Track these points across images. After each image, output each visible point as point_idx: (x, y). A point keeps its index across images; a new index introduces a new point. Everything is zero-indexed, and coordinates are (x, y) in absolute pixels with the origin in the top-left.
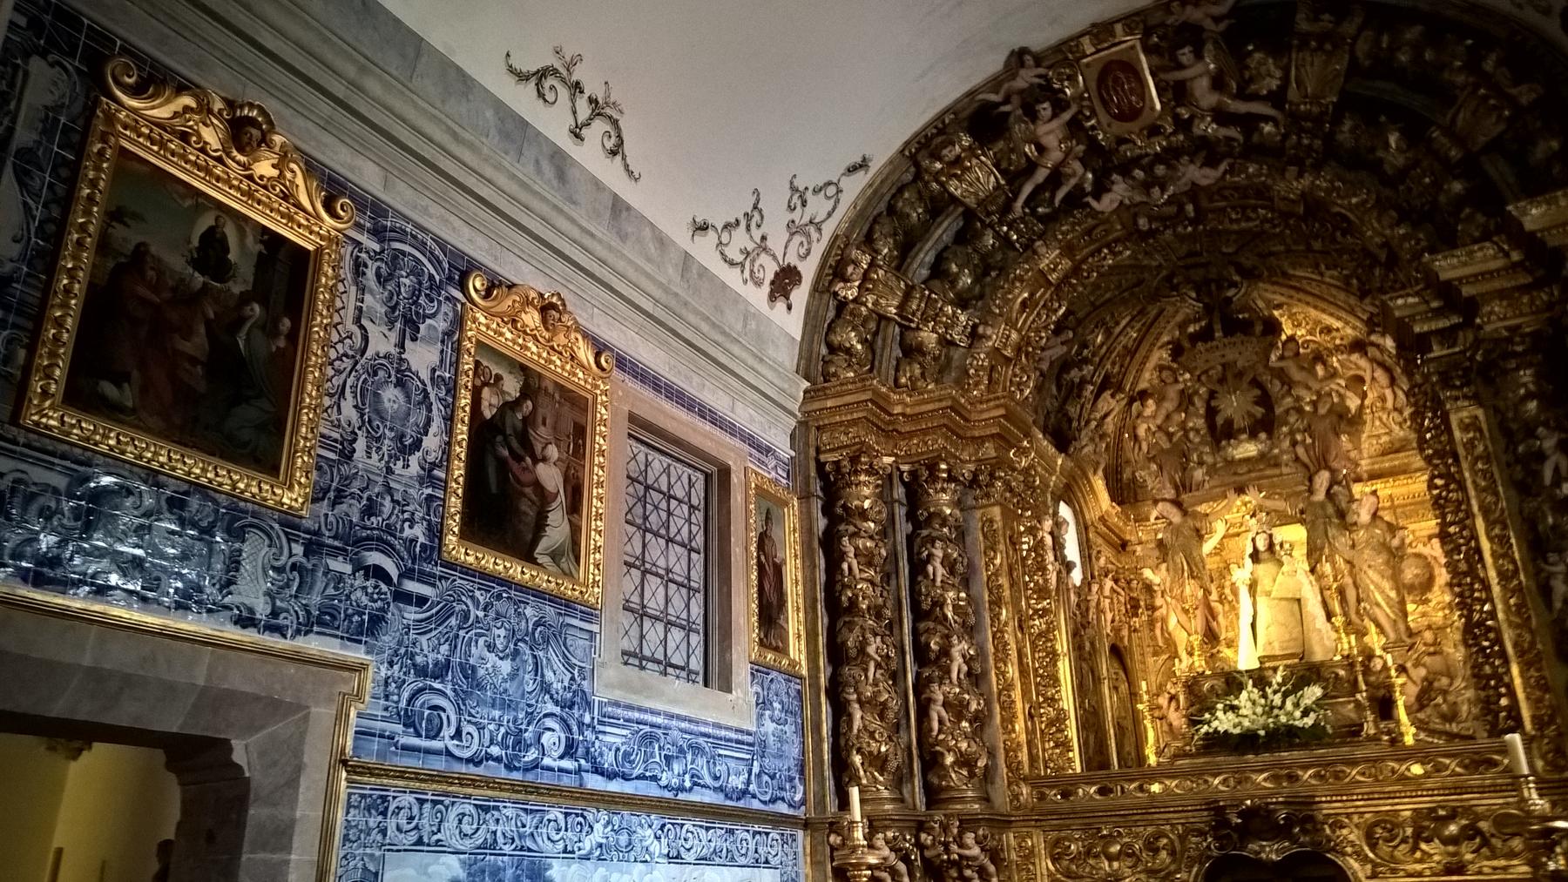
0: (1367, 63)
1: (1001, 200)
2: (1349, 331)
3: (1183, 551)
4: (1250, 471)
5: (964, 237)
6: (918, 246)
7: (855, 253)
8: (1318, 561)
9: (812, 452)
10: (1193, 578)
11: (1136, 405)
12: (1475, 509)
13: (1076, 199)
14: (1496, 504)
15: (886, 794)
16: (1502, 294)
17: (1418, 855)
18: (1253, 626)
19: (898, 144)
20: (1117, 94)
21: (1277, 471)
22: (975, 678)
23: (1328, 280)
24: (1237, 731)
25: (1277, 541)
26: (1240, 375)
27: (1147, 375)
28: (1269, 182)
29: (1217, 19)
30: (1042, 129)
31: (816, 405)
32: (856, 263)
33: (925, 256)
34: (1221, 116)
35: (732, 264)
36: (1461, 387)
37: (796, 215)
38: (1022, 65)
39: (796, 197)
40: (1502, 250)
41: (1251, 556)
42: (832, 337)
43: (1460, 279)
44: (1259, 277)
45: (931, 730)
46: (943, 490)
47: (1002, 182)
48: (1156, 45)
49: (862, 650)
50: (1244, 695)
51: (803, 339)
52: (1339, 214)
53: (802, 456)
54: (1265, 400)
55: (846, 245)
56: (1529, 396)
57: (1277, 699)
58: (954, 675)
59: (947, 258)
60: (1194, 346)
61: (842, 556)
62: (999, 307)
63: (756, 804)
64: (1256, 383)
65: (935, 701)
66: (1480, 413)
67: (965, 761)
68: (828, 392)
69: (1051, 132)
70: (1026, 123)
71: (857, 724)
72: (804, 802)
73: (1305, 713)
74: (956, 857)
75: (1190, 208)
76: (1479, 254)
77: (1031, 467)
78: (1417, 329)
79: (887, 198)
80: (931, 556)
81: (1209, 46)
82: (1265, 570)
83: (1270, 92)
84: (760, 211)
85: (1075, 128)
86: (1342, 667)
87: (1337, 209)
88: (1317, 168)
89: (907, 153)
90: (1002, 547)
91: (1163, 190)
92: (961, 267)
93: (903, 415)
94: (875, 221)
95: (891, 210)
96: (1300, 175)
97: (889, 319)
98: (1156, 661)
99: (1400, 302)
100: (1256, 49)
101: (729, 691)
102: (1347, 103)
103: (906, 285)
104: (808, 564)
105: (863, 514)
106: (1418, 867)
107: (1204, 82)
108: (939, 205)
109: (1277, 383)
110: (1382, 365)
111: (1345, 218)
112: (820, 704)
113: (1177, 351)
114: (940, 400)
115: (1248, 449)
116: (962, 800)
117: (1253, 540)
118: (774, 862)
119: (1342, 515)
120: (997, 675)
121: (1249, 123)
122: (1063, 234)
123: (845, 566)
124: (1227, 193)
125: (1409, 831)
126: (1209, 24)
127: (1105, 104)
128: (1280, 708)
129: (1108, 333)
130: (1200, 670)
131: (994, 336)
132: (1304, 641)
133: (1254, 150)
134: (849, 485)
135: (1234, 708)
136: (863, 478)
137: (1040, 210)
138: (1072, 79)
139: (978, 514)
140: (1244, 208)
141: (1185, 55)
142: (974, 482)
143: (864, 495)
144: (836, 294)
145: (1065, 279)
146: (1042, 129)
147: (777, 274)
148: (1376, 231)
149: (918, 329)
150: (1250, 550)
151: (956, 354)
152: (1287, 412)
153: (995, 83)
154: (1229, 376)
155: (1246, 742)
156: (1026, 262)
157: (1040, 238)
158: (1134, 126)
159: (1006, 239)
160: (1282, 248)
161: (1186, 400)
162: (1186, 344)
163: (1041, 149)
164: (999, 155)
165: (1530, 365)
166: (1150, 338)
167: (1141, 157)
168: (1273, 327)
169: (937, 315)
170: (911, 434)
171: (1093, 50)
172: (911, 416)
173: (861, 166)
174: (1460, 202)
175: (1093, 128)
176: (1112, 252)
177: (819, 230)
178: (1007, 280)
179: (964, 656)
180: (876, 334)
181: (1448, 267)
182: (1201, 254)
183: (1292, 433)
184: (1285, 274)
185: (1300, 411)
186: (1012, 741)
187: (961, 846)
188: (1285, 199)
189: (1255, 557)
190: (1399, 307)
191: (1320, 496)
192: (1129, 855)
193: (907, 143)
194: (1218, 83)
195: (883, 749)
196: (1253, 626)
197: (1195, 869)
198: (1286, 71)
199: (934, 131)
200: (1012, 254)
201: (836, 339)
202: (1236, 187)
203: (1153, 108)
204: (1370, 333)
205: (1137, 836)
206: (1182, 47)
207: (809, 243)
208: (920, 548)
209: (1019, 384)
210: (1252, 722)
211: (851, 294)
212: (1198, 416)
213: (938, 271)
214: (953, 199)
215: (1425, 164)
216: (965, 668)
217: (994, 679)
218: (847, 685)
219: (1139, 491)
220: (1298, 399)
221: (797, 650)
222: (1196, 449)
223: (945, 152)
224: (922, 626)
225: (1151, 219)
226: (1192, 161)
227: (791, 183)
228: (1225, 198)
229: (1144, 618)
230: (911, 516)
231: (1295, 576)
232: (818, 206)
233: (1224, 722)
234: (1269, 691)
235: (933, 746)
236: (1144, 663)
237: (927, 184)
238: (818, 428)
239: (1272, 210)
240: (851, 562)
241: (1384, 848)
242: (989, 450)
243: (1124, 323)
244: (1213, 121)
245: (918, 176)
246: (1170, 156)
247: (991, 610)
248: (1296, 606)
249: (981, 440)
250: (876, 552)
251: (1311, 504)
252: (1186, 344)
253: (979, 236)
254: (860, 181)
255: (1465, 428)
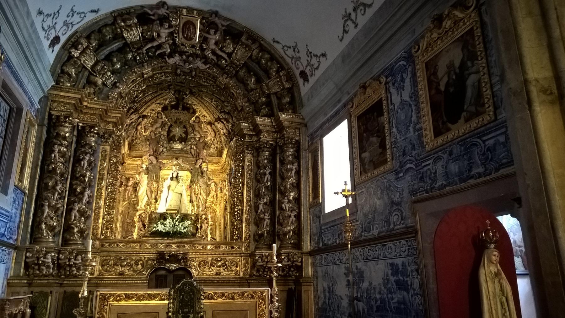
0: (254, 58)
1: (139, 45)
2: (209, 118)
3: (155, 173)
4: (179, 153)
5: (122, 50)
6: (104, 47)
7: (83, 41)
8: (193, 185)
9: (48, 109)
10: (156, 182)
11: (141, 119)
12: (245, 183)
13: (162, 55)
14: (250, 182)
15: (51, 240)
16: (267, 132)
17: (210, 270)
18: (166, 199)
19: (111, 9)
20: (188, 31)
21: (187, 155)
22: (89, 203)
23: (212, 104)
24: (164, 231)
25: (179, 175)
26: (181, 122)
27: (147, 111)
28: (218, 76)
29: (223, 26)
30: (162, 31)
31: (55, 92)
32: (82, 44)
33: (106, 51)
34: (214, 53)
35: (44, 29)
36: (250, 151)
37: (68, 19)
38: (163, 7)
39: (72, 12)
40: (272, 121)
41: (171, 178)
42: (64, 68)
43: (260, 124)
44: (194, 95)
45: (71, 219)
46: (93, 136)
47: (141, 39)
48: (204, 23)
49: (54, 187)
50: (168, 221)
51: (53, 64)
52: (233, 93)
53: (43, 110)
54: (186, 133)
55: (81, 37)
56: (267, 159)
57: (177, 223)
58: (84, 202)
59: (113, 56)
60: (171, 110)
61: (53, 151)
62: (125, 79)
63: (5, 240)
64: (185, 127)
65: (74, 209)
66: (252, 159)
67: (81, 232)
68: (62, 89)
69: (164, 33)
70: (158, 26)
71: (46, 214)
72: (17, 240)
73: (184, 228)
74: (72, 263)
75: (194, 73)
76: (267, 120)
77: (121, 135)
78: (244, 132)
79: (100, 26)
80: (84, 159)
81: (219, 32)
82: (174, 183)
83: (228, 53)
84: (59, 13)
85: (171, 34)
86: (194, 216)
87: (232, 91)
88: (231, 78)
89: (113, 15)
90: (107, 160)
91: (189, 65)
92: (118, 61)
93: (86, 106)
94: (93, 32)
95: (100, 31)
96: (227, 78)
97: (87, 69)
98: (123, 203)
99: (244, 124)
100: (229, 39)
101: (7, 196)
102: (245, 65)
103: (97, 59)
104: (37, 151)
105: (65, 138)
106: (209, 273)
107: (213, 41)
108: (118, 37)
109: (191, 128)
110: (214, 130)
111: (233, 94)
112: (31, 204)
113: (165, 109)
114: (102, 106)
115: (178, 146)
116: (77, 244)
117: (173, 174)
118: (5, 261)
119: (202, 173)
120: (95, 203)
121: (219, 57)
122: (154, 64)
123: (53, 155)
124: (205, 73)
125: (210, 263)
126: (220, 26)
127: (183, 32)
128: (177, 226)
129: (144, 95)
130: (153, 211)
131: (122, 88)
132: (180, 206)
133: (218, 66)
134: (62, 126)
135: (164, 224)
136: (67, 125)
137: (150, 53)
138: (176, 19)
139: (101, 147)
140: (207, 79)
141: (212, 31)
142: (103, 136)
143: (66, 131)
144: (71, 52)
145: (148, 78)
146: (162, 31)
147: (54, 38)
148: (241, 102)
149: (96, 76)
150: (171, 176)
151: (106, 89)
152: (191, 138)
153: (151, 7)
154: (177, 122)
155: (167, 235)
156: (139, 68)
157: (146, 62)
158: (189, 43)
159: (135, 58)
160: (206, 91)
161: (163, 125)
162: (169, 108)
163: (159, 35)
164: (144, 31)
165: (269, 151)
166: (153, 100)
167: (186, 52)
168: (194, 112)
169: (104, 74)
170: (85, 114)
171: (186, 14)
172: (89, 107)
173: (96, 11)
174: (263, 103)
175: (176, 37)
176: (165, 75)
177: (72, 27)
178: (131, 71)
179: (88, 195)
180: (80, 72)
181: (259, 120)
182: (184, 83)
183: (191, 144)
184: (202, 98)
185: (195, 139)
186: (96, 226)
187: (75, 259)
188: (221, 82)
189: (172, 179)
190: (243, 125)
191: (198, 166)
192: (129, 266)
193: (114, 11)
194: (216, 43)
195: (55, 224)
196: (166, 199)
197: (149, 271)
198: (235, 49)
199: (125, 12)
200: (134, 63)
201: (66, 69)
202: (209, 73)
203: (196, 40)
204: (216, 121)
205: (133, 260)
206: (212, 29)
207: (67, 30)
208: (80, 154)
209: (123, 107)
210: (169, 229)
211: (77, 55)
212: (165, 131)
213: (108, 58)
214: (123, 37)
215: (258, 90)
216: (88, 200)
217: (94, 204)
218: (46, 199)
219: (132, 147)
220: (195, 135)
221: (26, 183)
222: (162, 141)
223: (128, 22)
224: (74, 182)
225: (181, 71)
226: (200, 60)
227: (72, 8)
228: (204, 74)
229: (123, 188)
230: (78, 142)
231: (182, 187)
232: (76, 19)
233: (160, 228)
234: (175, 220)
235: (71, 224)
236: (119, 203)
237: (116, 28)
238: (52, 101)
239: (215, 83)
240: (56, 155)
241: (202, 268)
242: (110, 127)
243: (149, 93)
244: (211, 53)
245: (113, 24)
246: (195, 56)
247: (99, 181)
248: (180, 195)
249: (109, 122)
250: (67, 153)
251: (195, 168)
252: (169, 108)
253: (127, 53)
254: (94, 16)
255: (249, 162)
